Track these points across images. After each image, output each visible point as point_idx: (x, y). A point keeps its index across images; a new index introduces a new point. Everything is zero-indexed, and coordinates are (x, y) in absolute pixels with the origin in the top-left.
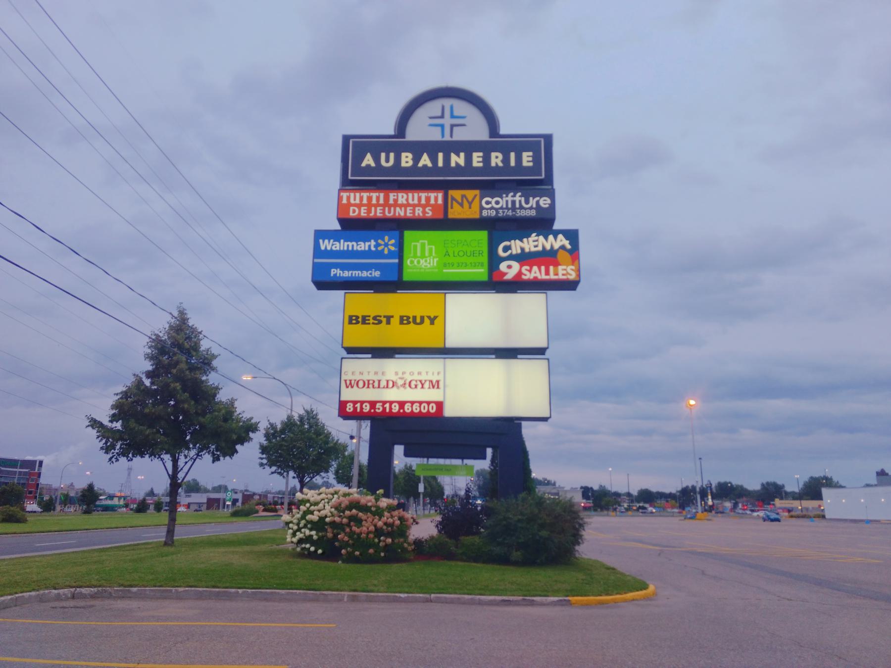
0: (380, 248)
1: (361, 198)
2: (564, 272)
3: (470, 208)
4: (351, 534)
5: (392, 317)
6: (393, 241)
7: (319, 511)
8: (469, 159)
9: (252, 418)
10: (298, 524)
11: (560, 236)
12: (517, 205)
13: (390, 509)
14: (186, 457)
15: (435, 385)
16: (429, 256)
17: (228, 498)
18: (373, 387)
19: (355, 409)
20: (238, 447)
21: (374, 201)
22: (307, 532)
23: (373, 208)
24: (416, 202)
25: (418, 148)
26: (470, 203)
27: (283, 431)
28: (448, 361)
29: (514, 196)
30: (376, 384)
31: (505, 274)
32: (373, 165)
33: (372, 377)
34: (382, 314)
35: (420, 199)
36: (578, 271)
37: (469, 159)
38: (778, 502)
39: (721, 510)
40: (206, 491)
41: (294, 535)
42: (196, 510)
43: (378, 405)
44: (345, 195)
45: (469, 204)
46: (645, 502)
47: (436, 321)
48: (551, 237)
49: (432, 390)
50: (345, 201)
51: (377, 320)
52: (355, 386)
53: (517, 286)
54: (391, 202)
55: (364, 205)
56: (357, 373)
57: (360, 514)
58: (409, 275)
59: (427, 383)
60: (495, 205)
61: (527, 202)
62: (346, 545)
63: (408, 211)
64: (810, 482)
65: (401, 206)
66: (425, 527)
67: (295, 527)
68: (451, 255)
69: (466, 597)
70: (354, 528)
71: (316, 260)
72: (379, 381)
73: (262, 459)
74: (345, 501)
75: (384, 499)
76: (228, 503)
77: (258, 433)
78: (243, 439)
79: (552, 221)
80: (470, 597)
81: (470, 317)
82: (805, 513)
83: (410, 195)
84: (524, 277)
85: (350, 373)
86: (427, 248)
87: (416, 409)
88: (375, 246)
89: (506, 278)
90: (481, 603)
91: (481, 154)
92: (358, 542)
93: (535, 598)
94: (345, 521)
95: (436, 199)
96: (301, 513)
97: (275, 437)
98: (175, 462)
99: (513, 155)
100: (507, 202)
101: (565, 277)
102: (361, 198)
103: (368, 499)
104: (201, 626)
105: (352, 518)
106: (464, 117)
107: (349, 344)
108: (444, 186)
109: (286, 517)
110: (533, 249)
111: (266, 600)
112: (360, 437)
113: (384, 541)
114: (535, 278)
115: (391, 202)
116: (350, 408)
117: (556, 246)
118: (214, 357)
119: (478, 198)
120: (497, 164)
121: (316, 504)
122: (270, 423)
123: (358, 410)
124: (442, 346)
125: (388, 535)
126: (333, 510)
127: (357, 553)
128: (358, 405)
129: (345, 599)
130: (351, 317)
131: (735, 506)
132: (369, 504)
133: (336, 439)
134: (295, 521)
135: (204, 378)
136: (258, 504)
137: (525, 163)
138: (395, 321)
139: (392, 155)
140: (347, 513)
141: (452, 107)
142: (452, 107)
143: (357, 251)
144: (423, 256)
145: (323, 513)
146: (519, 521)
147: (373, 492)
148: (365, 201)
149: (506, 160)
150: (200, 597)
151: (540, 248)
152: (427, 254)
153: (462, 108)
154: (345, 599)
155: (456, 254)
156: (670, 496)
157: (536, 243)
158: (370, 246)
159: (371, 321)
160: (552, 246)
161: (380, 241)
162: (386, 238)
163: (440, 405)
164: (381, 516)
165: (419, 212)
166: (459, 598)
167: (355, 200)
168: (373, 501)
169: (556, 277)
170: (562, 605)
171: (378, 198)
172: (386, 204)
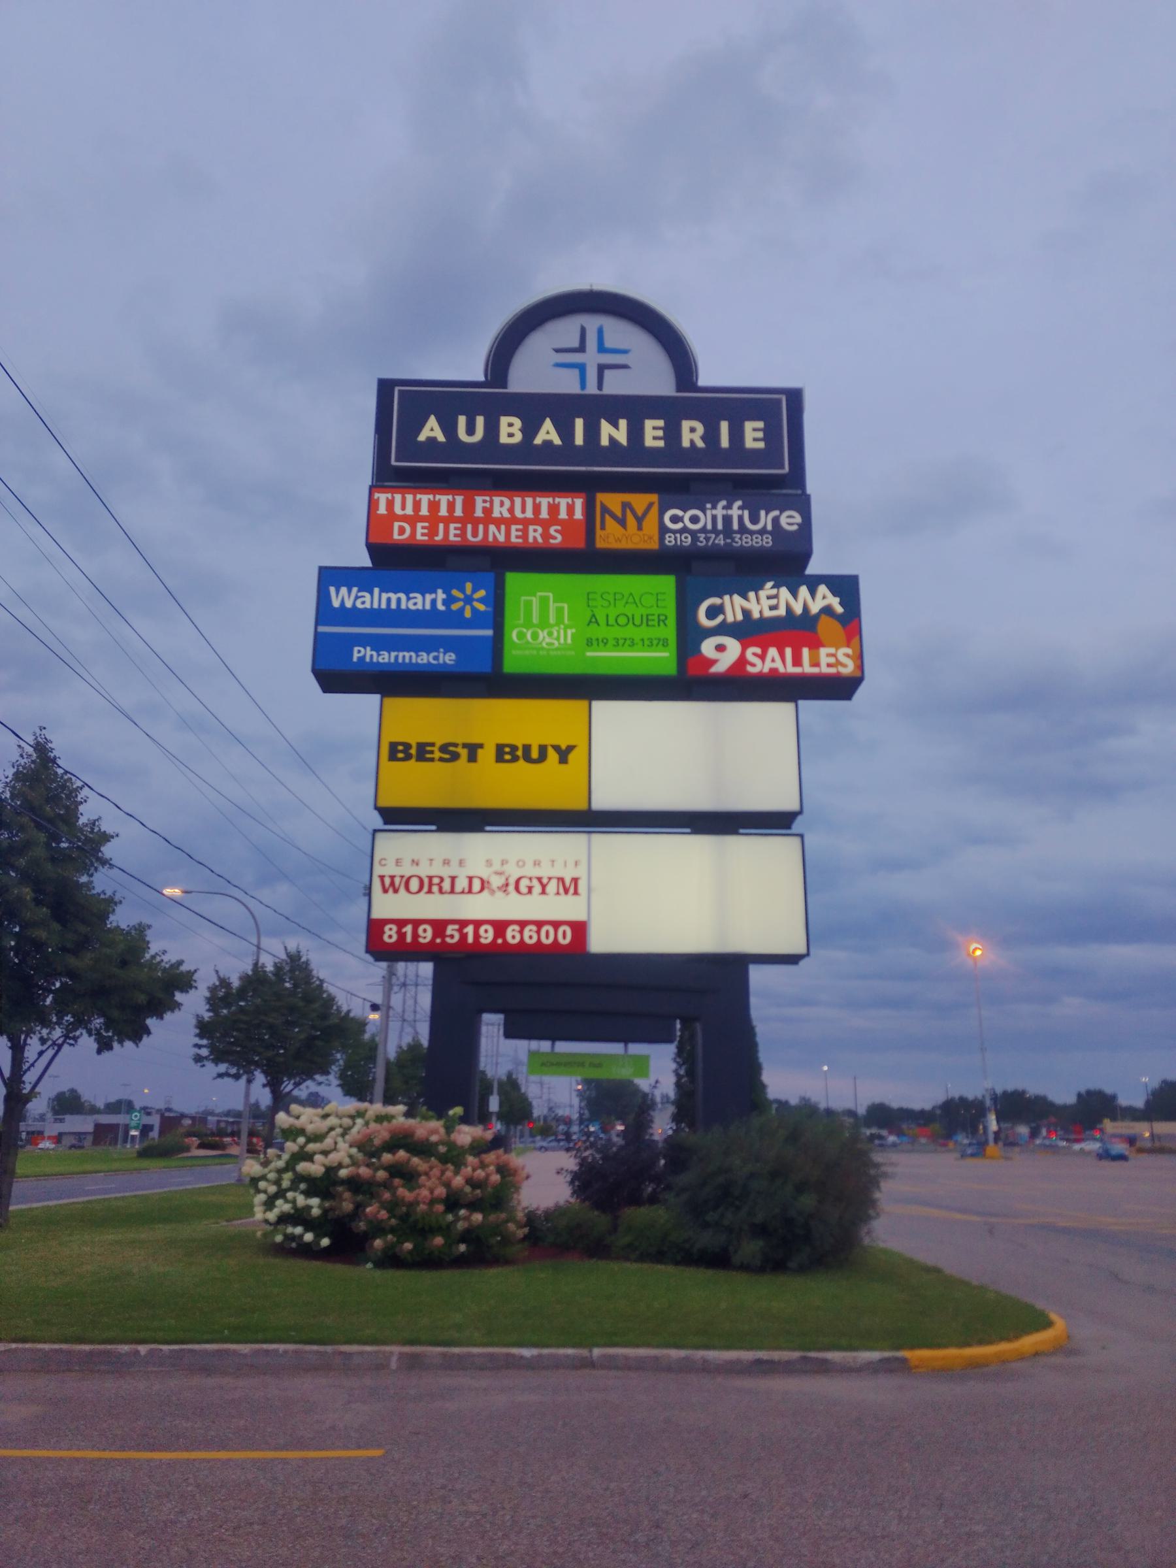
0: (455, 607)
1: (417, 505)
2: (832, 660)
3: (640, 528)
4: (392, 1206)
5: (481, 746)
6: (482, 593)
7: (325, 1153)
8: (636, 433)
9: (180, 963)
10: (277, 1182)
11: (822, 589)
12: (735, 526)
13: (479, 1148)
14: (43, 1041)
15: (569, 887)
16: (557, 624)
17: (133, 1124)
18: (441, 891)
19: (402, 936)
20: (151, 1022)
21: (443, 512)
22: (301, 1200)
23: (441, 526)
24: (529, 514)
25: (533, 409)
26: (640, 520)
27: (242, 992)
28: (595, 837)
29: (728, 507)
30: (446, 885)
31: (713, 662)
32: (441, 438)
33: (437, 870)
34: (460, 741)
35: (537, 508)
36: (859, 658)
37: (636, 433)
38: (1109, 1126)
39: (1011, 1139)
40: (94, 1110)
41: (269, 1204)
42: (73, 1146)
43: (450, 930)
44: (382, 498)
45: (637, 521)
46: (881, 1127)
47: (572, 757)
48: (804, 591)
49: (563, 898)
50: (382, 510)
51: (449, 753)
52: (402, 890)
53: (739, 687)
54: (479, 513)
55: (423, 519)
56: (407, 862)
57: (415, 1160)
58: (515, 660)
59: (554, 883)
60: (688, 523)
61: (755, 519)
62: (378, 1229)
63: (514, 533)
64: (1161, 1088)
65: (498, 522)
66: (545, 1181)
67: (273, 1189)
68: (602, 621)
69: (674, 1353)
70: (402, 1192)
71: (321, 629)
72: (453, 879)
73: (199, 1046)
74: (382, 1133)
75: (465, 1128)
76: (134, 1133)
77: (192, 992)
78: (161, 1005)
79: (805, 556)
80: (683, 1353)
81: (640, 750)
82: (1157, 1144)
83: (518, 501)
84: (750, 669)
85: (391, 863)
86: (552, 606)
87: (530, 936)
88: (445, 602)
89: (714, 669)
90: (707, 1368)
91: (660, 423)
92: (411, 1224)
93: (830, 1355)
94: (381, 1175)
95: (571, 509)
96: (286, 1157)
97: (228, 1005)
98: (17, 1049)
99: (724, 426)
100: (714, 518)
101: (832, 670)
102: (417, 505)
103: (429, 1128)
104: (35, 1463)
105: (396, 1171)
106: (625, 352)
107: (390, 800)
108: (587, 485)
109: (252, 1167)
110: (768, 613)
111: (207, 1371)
112: (389, 1007)
113: (466, 1218)
114: (774, 671)
115: (479, 513)
116: (390, 935)
117: (815, 608)
118: (106, 838)
119: (655, 510)
120: (692, 442)
121: (318, 1138)
122: (219, 978)
123: (409, 939)
124: (581, 805)
125: (473, 1206)
126: (354, 1151)
127: (408, 1246)
128: (408, 929)
129: (394, 1364)
130: (393, 747)
131: (1034, 1134)
132: (434, 1138)
133: (345, 1009)
134: (272, 1176)
135: (84, 879)
136: (190, 1134)
137: (749, 444)
138: (487, 755)
139: (480, 421)
140: (387, 1157)
141: (600, 332)
142: (600, 332)
143: (408, 609)
144: (544, 624)
145: (334, 1158)
146: (752, 1175)
147: (440, 1114)
148: (424, 511)
149: (711, 436)
150: (44, 1365)
151: (782, 612)
152: (552, 621)
153: (619, 332)
154: (394, 1364)
155: (612, 621)
156: (922, 1118)
157: (773, 602)
158: (434, 602)
159: (437, 755)
160: (806, 608)
161: (455, 593)
162: (469, 587)
163: (579, 929)
164: (458, 1164)
165: (535, 534)
166: (656, 1358)
167: (403, 507)
168: (442, 1131)
169: (815, 670)
170: (891, 1371)
171: (451, 506)
172: (469, 516)
